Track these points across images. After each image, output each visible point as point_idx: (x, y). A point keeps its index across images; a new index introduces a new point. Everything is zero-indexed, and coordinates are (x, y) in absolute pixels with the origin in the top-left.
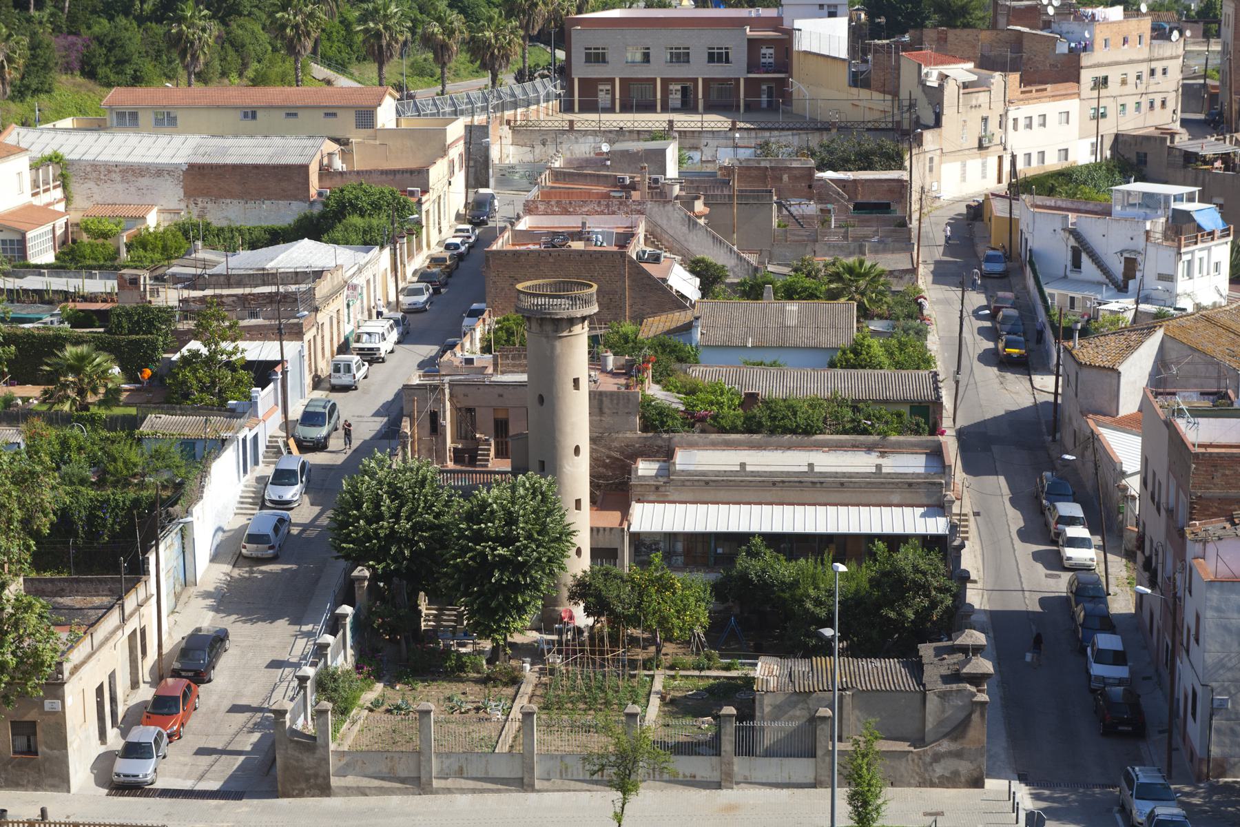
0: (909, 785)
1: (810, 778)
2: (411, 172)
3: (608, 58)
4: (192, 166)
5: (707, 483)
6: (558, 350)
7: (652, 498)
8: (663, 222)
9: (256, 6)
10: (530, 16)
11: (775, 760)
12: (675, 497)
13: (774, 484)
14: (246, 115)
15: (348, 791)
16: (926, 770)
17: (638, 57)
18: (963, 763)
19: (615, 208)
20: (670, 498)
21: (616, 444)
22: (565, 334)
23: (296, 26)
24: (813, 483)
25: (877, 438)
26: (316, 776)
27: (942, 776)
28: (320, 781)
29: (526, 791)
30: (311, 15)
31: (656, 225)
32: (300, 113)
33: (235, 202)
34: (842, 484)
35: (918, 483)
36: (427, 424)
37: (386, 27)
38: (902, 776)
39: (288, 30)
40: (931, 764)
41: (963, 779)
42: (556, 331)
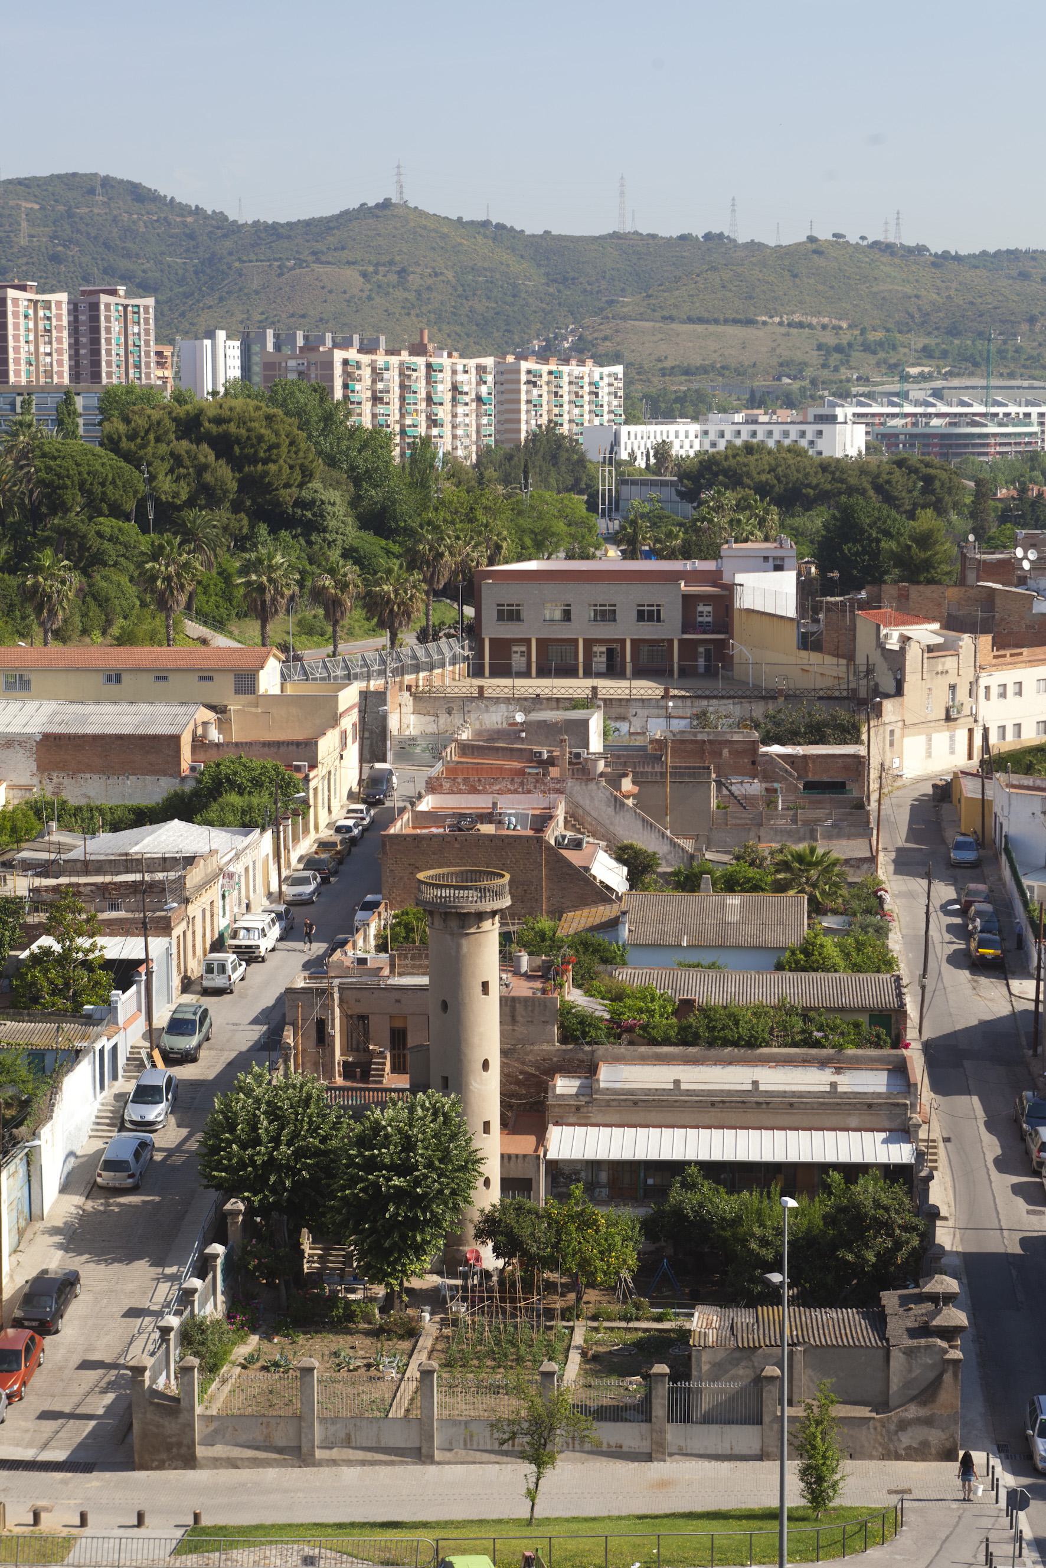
0: (871, 1457)
1: (755, 1449)
2: (298, 744)
3: (524, 615)
4: (46, 737)
5: (635, 1103)
6: (465, 950)
7: (571, 1120)
8: (586, 803)
9: (123, 556)
10: (434, 567)
11: (715, 1428)
12: (599, 1119)
13: (713, 1104)
14: (109, 679)
15: (216, 1463)
16: (891, 1440)
17: (558, 615)
18: (934, 1431)
19: (531, 787)
20: (594, 1121)
21: (530, 1058)
22: (472, 930)
23: (168, 579)
24: (758, 1103)
25: (832, 1051)
26: (179, 1444)
27: (909, 1448)
28: (184, 1450)
29: (424, 1463)
30: (186, 566)
31: (577, 805)
32: (171, 676)
33: (96, 777)
34: (791, 1105)
35: (880, 1104)
36: (313, 1033)
37: (271, 580)
38: (862, 1447)
39: (159, 583)
40: (896, 1432)
41: (933, 1451)
42: (463, 927)
